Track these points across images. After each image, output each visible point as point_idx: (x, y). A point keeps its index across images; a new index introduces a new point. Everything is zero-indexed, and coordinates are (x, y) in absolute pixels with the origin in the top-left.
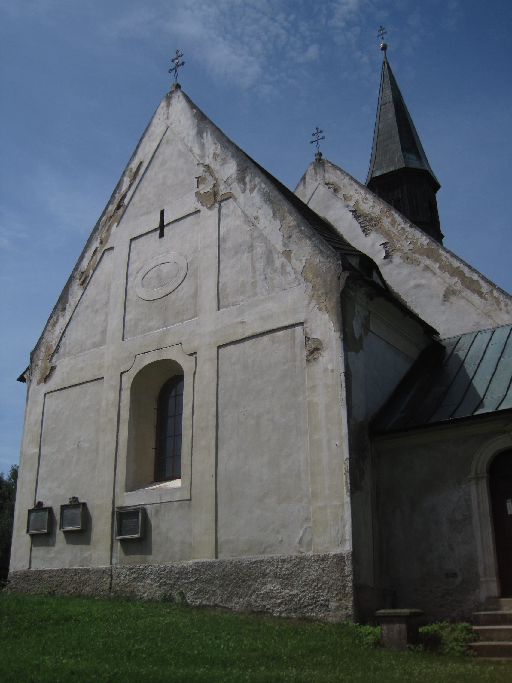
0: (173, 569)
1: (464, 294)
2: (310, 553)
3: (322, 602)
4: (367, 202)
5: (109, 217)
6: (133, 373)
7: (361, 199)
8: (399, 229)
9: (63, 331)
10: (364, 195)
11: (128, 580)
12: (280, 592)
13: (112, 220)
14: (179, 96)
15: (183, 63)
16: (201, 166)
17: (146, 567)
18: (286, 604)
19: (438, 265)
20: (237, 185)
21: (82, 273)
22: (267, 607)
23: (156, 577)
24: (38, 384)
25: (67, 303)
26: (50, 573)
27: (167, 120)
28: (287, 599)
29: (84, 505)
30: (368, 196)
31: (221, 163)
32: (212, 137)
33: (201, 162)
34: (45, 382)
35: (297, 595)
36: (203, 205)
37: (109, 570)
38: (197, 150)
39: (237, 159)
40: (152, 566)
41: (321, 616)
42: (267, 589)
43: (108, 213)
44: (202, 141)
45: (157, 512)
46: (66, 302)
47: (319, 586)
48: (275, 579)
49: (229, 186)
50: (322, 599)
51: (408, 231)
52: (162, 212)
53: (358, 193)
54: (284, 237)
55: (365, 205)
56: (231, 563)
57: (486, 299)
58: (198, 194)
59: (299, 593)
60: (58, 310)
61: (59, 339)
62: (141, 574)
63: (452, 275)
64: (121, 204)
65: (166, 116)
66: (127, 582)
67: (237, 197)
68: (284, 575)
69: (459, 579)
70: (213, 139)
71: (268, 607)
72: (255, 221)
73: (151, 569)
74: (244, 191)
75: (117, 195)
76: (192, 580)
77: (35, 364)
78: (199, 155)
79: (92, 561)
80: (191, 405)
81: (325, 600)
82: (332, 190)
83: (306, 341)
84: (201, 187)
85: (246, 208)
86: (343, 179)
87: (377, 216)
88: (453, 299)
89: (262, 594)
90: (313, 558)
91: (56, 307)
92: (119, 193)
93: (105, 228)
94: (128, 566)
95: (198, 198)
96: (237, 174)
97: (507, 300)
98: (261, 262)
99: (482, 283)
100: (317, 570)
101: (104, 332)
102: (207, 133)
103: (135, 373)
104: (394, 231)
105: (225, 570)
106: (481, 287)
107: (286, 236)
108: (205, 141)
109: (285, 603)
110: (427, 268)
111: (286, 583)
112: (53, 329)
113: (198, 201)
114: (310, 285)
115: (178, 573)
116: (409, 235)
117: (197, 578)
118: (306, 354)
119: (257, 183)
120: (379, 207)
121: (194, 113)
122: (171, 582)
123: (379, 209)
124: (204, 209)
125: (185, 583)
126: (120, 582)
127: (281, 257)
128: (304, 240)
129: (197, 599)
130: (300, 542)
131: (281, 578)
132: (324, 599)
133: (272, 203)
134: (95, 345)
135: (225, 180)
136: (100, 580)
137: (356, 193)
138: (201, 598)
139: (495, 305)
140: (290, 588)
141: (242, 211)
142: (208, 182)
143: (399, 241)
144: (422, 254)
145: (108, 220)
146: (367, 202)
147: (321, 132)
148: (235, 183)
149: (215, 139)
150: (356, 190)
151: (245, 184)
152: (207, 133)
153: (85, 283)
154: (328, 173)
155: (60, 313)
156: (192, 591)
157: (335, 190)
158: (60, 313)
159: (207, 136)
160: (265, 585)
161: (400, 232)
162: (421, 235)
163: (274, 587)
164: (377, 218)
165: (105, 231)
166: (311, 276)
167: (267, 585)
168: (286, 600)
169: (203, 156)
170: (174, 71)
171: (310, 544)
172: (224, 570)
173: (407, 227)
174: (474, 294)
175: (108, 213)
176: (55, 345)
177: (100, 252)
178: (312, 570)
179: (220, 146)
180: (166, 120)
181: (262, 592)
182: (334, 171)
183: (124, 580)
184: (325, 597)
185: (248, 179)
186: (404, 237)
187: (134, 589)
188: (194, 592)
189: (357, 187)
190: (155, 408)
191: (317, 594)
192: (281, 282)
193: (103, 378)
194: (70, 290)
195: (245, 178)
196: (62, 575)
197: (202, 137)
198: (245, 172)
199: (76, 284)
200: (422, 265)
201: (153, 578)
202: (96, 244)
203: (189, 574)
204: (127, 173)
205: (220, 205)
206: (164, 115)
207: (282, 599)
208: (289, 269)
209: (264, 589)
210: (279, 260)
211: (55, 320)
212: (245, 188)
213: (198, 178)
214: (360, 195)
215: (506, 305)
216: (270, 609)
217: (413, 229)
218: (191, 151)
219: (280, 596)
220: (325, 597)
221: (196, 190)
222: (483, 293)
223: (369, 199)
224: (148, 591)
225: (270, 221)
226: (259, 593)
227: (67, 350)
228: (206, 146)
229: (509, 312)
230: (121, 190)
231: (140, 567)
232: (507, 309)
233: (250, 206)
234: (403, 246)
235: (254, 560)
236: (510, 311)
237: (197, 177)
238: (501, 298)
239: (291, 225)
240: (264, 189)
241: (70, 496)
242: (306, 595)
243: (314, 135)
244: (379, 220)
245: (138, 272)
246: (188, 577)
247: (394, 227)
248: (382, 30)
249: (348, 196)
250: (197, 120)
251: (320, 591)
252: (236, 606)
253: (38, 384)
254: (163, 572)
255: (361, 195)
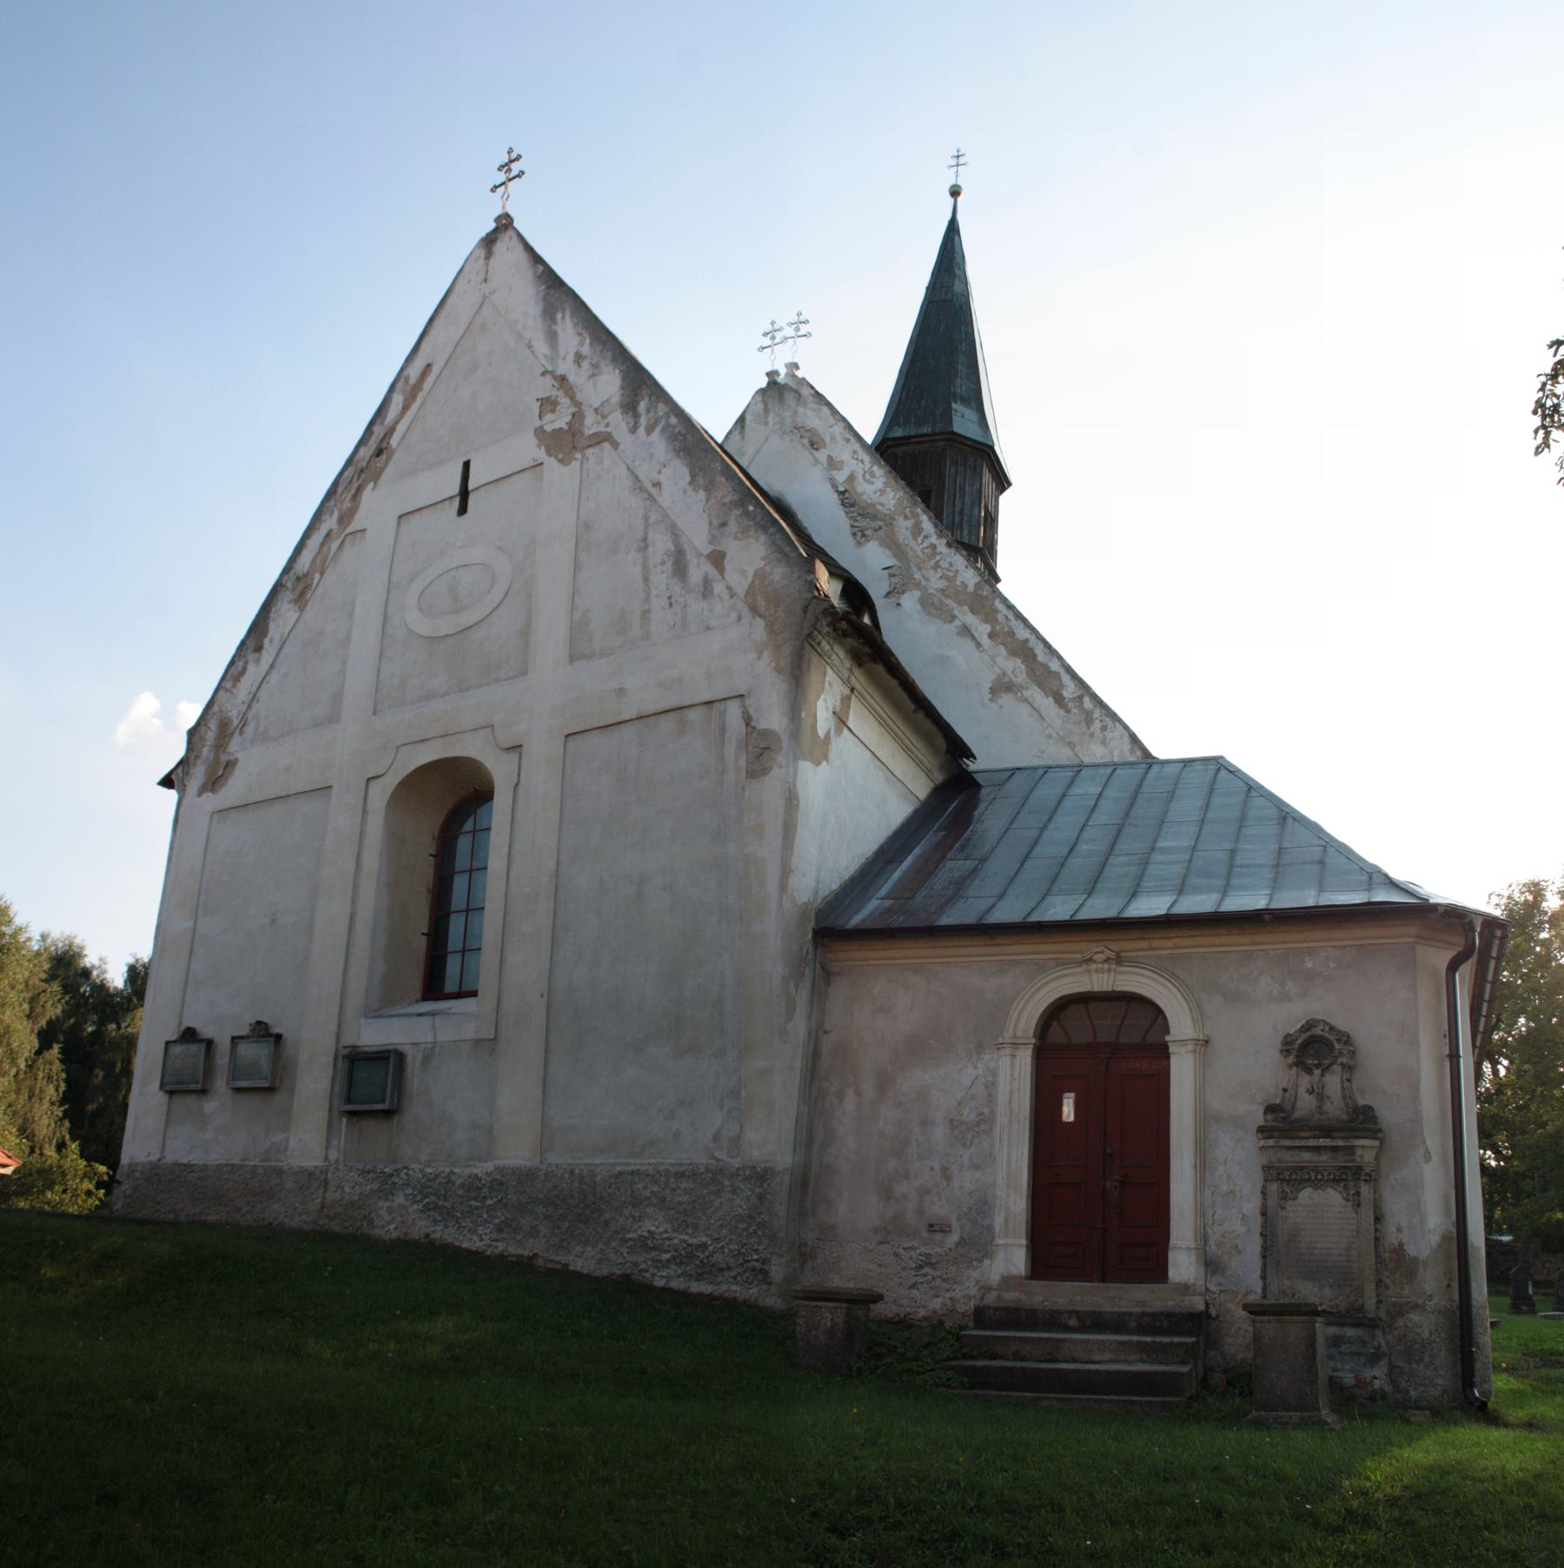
0: (453, 1178)
1: (1027, 693)
2: (735, 1163)
3: (755, 1264)
4: (872, 480)
5: (359, 470)
6: (392, 781)
7: (860, 472)
8: (925, 544)
9: (254, 689)
10: (868, 465)
11: (360, 1194)
12: (669, 1239)
13: (363, 477)
14: (511, 238)
15: (521, 174)
16: (548, 377)
17: (396, 1170)
18: (681, 1263)
19: (987, 628)
20: (620, 417)
21: (298, 578)
22: (640, 1267)
23: (415, 1193)
24: (200, 794)
25: (265, 636)
26: (201, 1170)
27: (483, 284)
28: (683, 1253)
29: (278, 1037)
30: (875, 468)
31: (590, 372)
32: (574, 320)
33: (550, 369)
34: (213, 790)
35: (704, 1246)
36: (549, 454)
37: (321, 1172)
38: (541, 347)
39: (622, 365)
40: (408, 1169)
41: (751, 1291)
42: (643, 1229)
43: (358, 462)
44: (554, 327)
45: (426, 1060)
46: (264, 633)
47: (751, 1230)
48: (661, 1209)
49: (604, 417)
50: (755, 1257)
51: (941, 553)
52: (467, 465)
53: (857, 459)
54: (711, 523)
55: (866, 485)
56: (572, 1173)
57: (1068, 711)
58: (540, 433)
59: (709, 1243)
60: (247, 649)
61: (246, 706)
62: (386, 1184)
63: (1013, 653)
64: (384, 445)
65: (482, 276)
66: (357, 1197)
67: (619, 441)
68: (680, 1203)
69: (954, 1238)
70: (576, 325)
71: (643, 1266)
72: (654, 491)
73: (407, 1175)
74: (634, 430)
75: (376, 429)
76: (489, 1202)
77: (194, 754)
78: (545, 356)
79: (289, 1152)
80: (505, 850)
81: (762, 1261)
82: (806, 441)
83: (747, 733)
84: (549, 417)
85: (637, 463)
86: (832, 426)
87: (886, 512)
88: (1006, 699)
89: (631, 1239)
90: (741, 1173)
91: (243, 643)
92: (382, 424)
93: (350, 491)
94: (360, 1166)
95: (539, 441)
96: (622, 395)
97: (1107, 719)
98: (663, 572)
99: (1066, 679)
100: (748, 1198)
101: (337, 698)
102: (563, 312)
103: (397, 781)
104: (916, 547)
105: (558, 1186)
106: (1062, 686)
107: (716, 522)
108: (558, 328)
109: (678, 1261)
110: (966, 631)
111: (682, 1219)
112: (234, 686)
113: (539, 446)
114: (760, 622)
115: (462, 1186)
116: (942, 561)
117: (499, 1198)
118: (747, 761)
119: (661, 414)
120: (893, 494)
121: (540, 271)
122: (446, 1204)
123: (893, 499)
124: (551, 463)
125: (476, 1208)
126: (343, 1198)
127: (704, 564)
128: (752, 532)
129: (498, 1241)
130: (716, 1138)
131: (672, 1209)
132: (761, 1257)
133: (689, 454)
134: (318, 724)
135: (595, 406)
136: (302, 1190)
137: (853, 457)
138: (505, 1239)
139: (1083, 724)
140: (690, 1231)
141: (628, 468)
142: (562, 410)
143: (920, 569)
144: (960, 603)
145: (356, 476)
146: (872, 480)
147: (806, 322)
148: (616, 413)
149: (580, 325)
150: (855, 452)
151: (636, 416)
152: (563, 312)
153: (301, 600)
154: (805, 407)
155: (251, 656)
156: (488, 1225)
157: (812, 444)
158: (251, 656)
159: (563, 318)
160: (639, 1221)
161: (926, 551)
162: (966, 567)
163: (657, 1227)
164: (885, 515)
165: (348, 498)
166: (764, 604)
167: (643, 1222)
168: (681, 1254)
169: (553, 357)
170: (500, 190)
171: (736, 1141)
172: (556, 1187)
173: (942, 547)
174: (1048, 697)
175: (358, 462)
176: (237, 718)
177: (337, 539)
178: (738, 1197)
179: (590, 339)
180: (481, 283)
181: (630, 1236)
182: (817, 406)
183: (349, 1193)
184: (761, 1255)
185: (642, 406)
186: (932, 562)
187: (370, 1213)
188: (492, 1226)
189: (857, 446)
190: (431, 852)
191: (745, 1247)
192: (702, 611)
193: (331, 787)
194: (273, 610)
195: (638, 404)
196: (226, 1177)
197: (553, 321)
198: (638, 391)
199: (286, 600)
200: (957, 623)
201: (410, 1194)
202: (330, 523)
203: (484, 1190)
204: (399, 386)
205: (584, 455)
206: (478, 273)
207: (672, 1253)
208: (719, 588)
209: (638, 1228)
210: (698, 570)
211: (240, 669)
212: (636, 423)
213: (542, 399)
214: (860, 464)
215: (1104, 728)
216: (647, 1271)
217: (953, 551)
218: (530, 346)
219: (669, 1246)
220: (761, 1255)
221: (538, 423)
222: (1065, 698)
223: (877, 475)
224: (398, 1218)
225: (685, 491)
226: (627, 1236)
227: (261, 730)
228: (562, 338)
229: (1107, 741)
230: (384, 419)
231: (385, 1170)
232: (1105, 737)
233: (644, 460)
234: (928, 580)
235: (619, 1168)
236: (1110, 740)
237: (540, 397)
238: (1097, 713)
239: (727, 500)
240: (674, 427)
241: (249, 1018)
242: (723, 1247)
243: (765, 334)
244: (889, 521)
245: (411, 581)
246: (482, 1195)
247: (916, 540)
248: (958, 156)
249: (837, 460)
250: (544, 287)
251: (753, 1240)
252: (577, 1259)
253: (200, 794)
254: (431, 1184)
255: (863, 463)
